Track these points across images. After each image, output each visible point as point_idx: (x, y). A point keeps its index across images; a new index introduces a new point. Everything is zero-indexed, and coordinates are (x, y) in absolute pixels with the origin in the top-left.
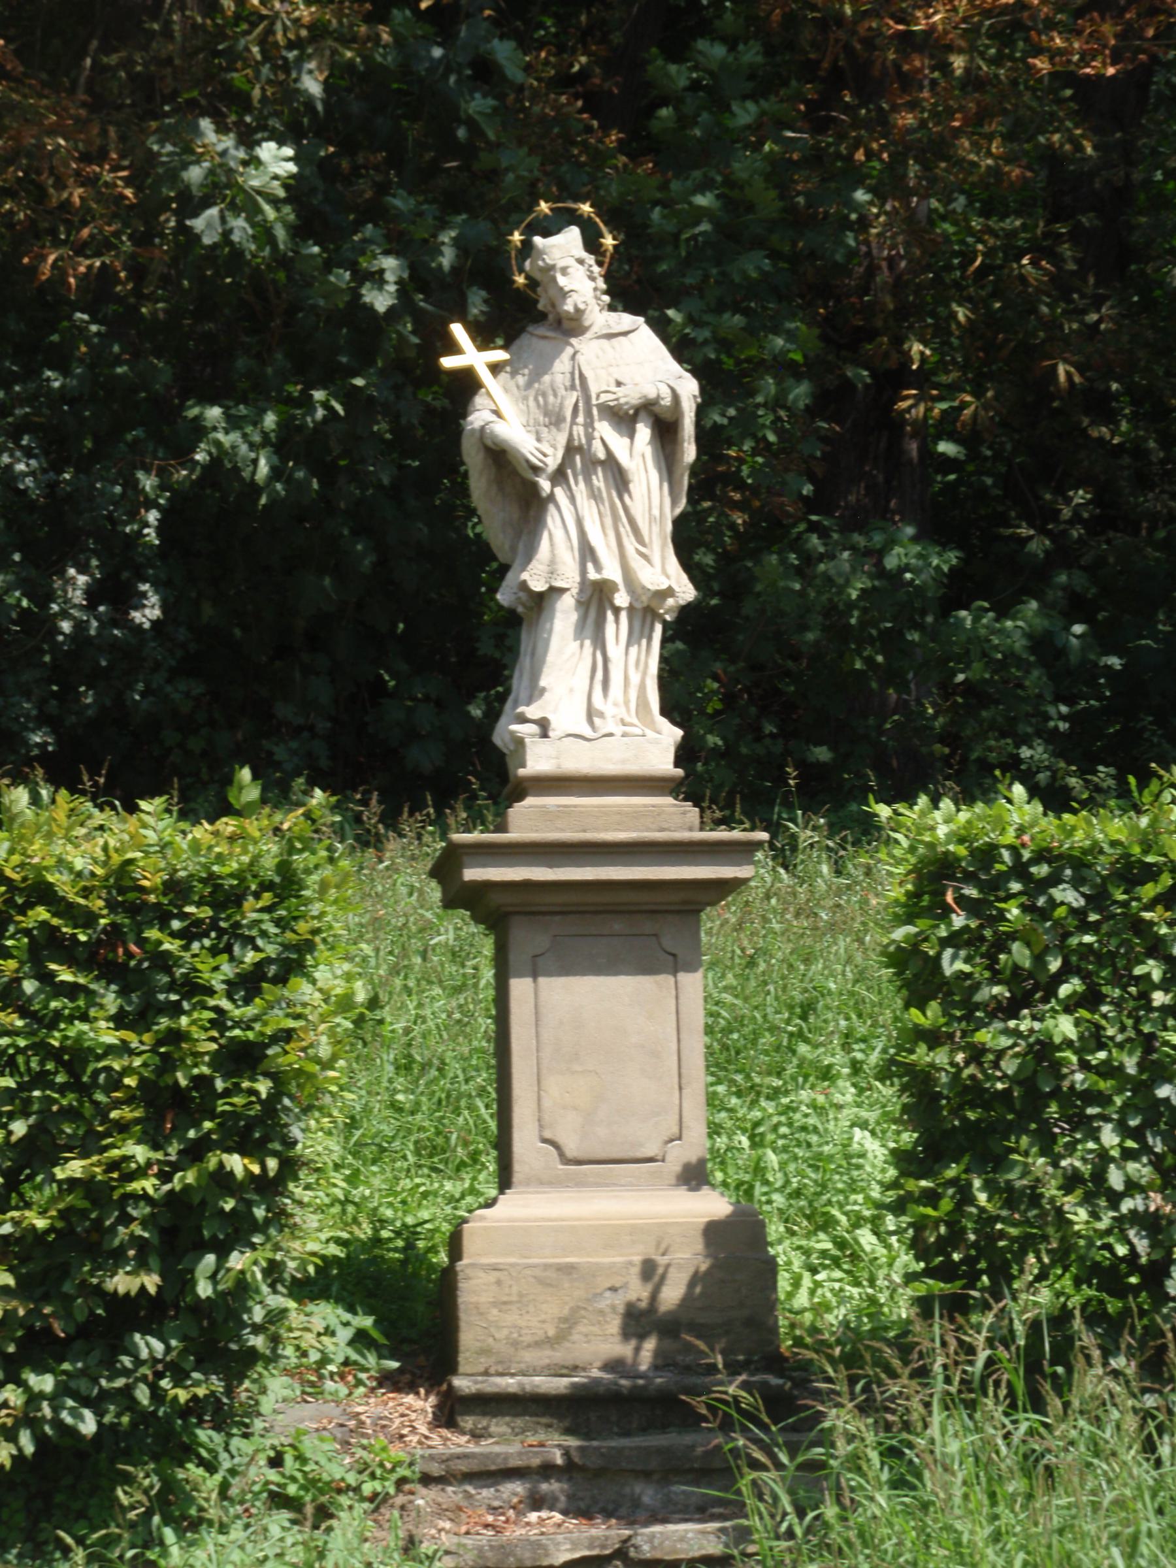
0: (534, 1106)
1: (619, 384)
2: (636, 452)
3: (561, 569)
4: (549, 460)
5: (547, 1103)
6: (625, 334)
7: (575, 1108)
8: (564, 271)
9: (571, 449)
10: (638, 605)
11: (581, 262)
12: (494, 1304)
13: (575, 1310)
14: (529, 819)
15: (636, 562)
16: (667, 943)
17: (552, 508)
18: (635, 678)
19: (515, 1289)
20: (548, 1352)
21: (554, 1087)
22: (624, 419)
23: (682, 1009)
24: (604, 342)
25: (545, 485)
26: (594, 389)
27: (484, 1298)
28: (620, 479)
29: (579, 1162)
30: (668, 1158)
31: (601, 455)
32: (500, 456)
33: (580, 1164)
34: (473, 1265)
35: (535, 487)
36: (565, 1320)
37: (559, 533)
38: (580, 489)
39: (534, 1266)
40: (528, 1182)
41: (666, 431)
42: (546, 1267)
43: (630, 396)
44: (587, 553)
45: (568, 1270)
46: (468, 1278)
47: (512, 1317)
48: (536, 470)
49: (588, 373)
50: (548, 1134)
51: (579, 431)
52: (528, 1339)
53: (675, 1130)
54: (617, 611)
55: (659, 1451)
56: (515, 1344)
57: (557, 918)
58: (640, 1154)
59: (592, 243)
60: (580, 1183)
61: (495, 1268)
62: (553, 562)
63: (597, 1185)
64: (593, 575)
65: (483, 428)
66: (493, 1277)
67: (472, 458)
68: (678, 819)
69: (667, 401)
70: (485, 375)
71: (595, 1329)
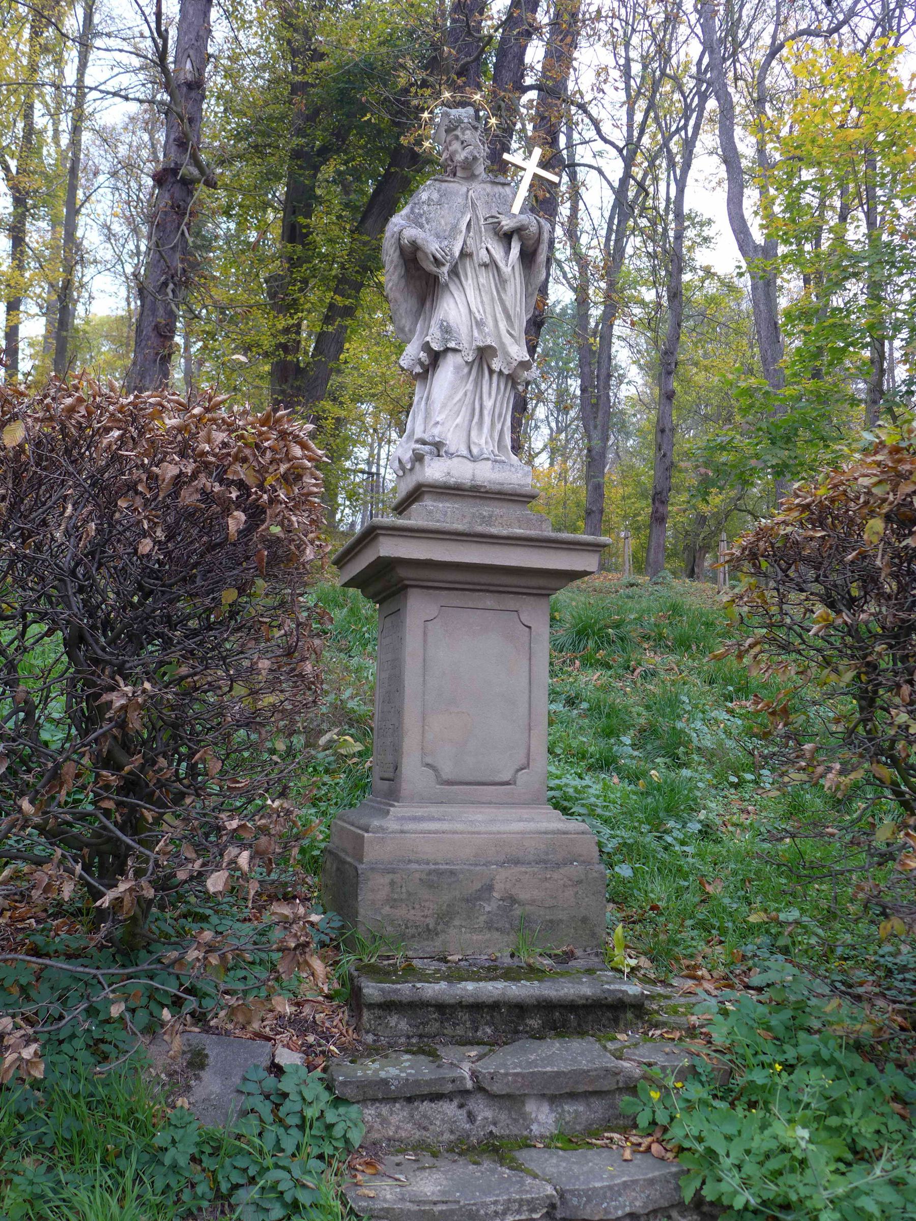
10: (506, 372)
16: (525, 618)
18: (499, 427)
28: (501, 281)
35: (436, 278)
48: (438, 263)
50: (429, 760)
53: (524, 761)
54: (491, 372)
58: (497, 779)
67: (390, 255)
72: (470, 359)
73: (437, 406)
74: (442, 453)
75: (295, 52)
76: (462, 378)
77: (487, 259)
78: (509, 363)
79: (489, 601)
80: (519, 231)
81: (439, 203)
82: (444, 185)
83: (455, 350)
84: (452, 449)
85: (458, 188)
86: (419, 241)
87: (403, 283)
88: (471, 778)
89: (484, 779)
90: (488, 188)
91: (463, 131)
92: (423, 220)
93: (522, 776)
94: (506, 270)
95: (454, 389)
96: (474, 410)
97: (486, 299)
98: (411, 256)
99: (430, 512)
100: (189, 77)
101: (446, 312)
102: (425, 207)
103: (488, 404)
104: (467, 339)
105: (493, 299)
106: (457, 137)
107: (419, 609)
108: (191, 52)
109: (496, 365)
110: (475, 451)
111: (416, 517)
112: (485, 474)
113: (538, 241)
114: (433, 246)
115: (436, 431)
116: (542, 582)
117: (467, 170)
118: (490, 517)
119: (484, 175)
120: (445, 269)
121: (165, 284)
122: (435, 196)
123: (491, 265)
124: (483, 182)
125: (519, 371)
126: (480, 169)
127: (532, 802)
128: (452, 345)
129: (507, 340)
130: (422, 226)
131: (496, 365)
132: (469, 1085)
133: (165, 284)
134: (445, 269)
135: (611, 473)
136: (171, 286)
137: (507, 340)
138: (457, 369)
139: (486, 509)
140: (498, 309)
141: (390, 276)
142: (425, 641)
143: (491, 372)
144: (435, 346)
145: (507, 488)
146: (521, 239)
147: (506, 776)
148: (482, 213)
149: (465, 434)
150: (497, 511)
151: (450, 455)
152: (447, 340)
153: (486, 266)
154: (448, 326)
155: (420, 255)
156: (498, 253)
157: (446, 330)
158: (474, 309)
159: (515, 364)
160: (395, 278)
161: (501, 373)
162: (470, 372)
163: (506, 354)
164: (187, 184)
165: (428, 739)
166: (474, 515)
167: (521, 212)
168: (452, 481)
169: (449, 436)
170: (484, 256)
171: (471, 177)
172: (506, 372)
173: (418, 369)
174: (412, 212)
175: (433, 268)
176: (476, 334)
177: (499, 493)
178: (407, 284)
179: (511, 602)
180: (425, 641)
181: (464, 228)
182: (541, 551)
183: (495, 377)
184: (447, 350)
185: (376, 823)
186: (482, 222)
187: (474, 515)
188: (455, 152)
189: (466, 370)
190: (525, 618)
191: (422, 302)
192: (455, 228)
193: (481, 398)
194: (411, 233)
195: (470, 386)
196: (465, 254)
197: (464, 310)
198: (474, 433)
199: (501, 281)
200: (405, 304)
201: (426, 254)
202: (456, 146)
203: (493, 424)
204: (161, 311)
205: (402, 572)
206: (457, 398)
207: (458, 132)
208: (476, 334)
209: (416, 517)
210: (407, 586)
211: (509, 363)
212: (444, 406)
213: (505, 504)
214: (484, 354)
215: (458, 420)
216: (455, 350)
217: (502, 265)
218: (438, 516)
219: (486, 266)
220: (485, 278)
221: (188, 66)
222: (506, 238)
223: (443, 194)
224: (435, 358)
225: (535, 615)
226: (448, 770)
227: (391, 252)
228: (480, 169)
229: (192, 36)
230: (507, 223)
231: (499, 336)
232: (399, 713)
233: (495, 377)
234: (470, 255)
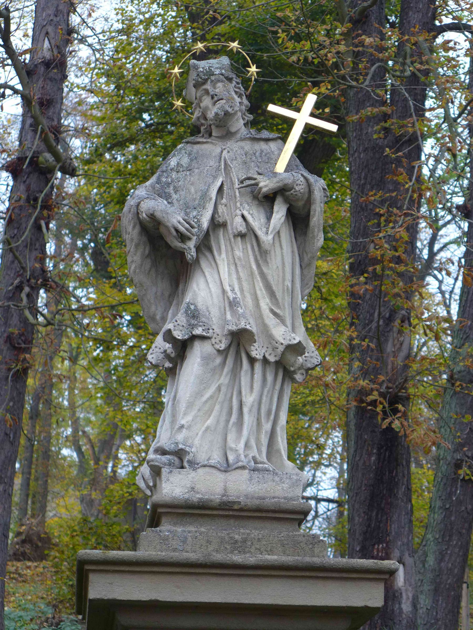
10: (272, 359)
18: (267, 427)
28: (262, 253)
35: (181, 254)
48: (183, 238)
54: (252, 361)
72: (222, 346)
73: (182, 406)
74: (186, 464)
75: (193, 18)
76: (214, 370)
77: (242, 228)
80: (282, 192)
81: (189, 169)
82: (196, 147)
83: (203, 338)
84: (202, 458)
85: (211, 149)
86: (158, 214)
87: (148, 264)
90: (247, 146)
91: (214, 84)
92: (171, 190)
94: (267, 239)
95: (203, 383)
96: (231, 408)
98: (153, 232)
99: (166, 539)
100: (48, 55)
101: (195, 294)
102: (174, 175)
103: (249, 399)
104: (218, 322)
105: (252, 274)
106: (207, 92)
108: (50, 29)
109: (257, 351)
110: (231, 458)
111: (151, 546)
112: (241, 487)
113: (309, 202)
114: (175, 218)
115: (180, 437)
117: (221, 128)
118: (244, 541)
119: (244, 131)
120: (191, 244)
121: (20, 288)
122: (185, 161)
123: (248, 234)
124: (242, 140)
125: (290, 358)
126: (238, 125)
128: (198, 331)
129: (271, 320)
130: (167, 197)
133: (20, 288)
134: (191, 244)
136: (27, 289)
137: (271, 320)
138: (206, 359)
139: (240, 532)
140: (259, 285)
143: (252, 361)
144: (179, 335)
145: (268, 503)
146: (286, 200)
148: (237, 174)
149: (219, 439)
150: (255, 533)
151: (193, 464)
152: (193, 327)
153: (242, 236)
154: (196, 309)
155: (162, 230)
156: (256, 219)
157: (194, 315)
158: (227, 288)
161: (265, 361)
162: (224, 362)
163: (270, 337)
164: (45, 173)
166: (222, 541)
167: (286, 171)
168: (196, 497)
169: (197, 442)
170: (238, 224)
171: (228, 135)
172: (272, 359)
173: (168, 365)
174: (159, 181)
175: (177, 244)
176: (229, 317)
177: (258, 510)
178: (155, 264)
181: (213, 193)
182: (304, 583)
183: (258, 367)
184: (194, 338)
186: (237, 186)
187: (222, 541)
188: (207, 108)
189: (218, 360)
192: (205, 196)
193: (240, 393)
194: (148, 206)
195: (224, 379)
196: (217, 225)
197: (215, 289)
198: (231, 437)
199: (262, 253)
200: (155, 288)
201: (167, 227)
202: (207, 102)
204: (15, 320)
206: (207, 395)
207: (208, 86)
208: (229, 317)
209: (151, 546)
212: (190, 405)
213: (268, 524)
214: (239, 340)
215: (209, 422)
216: (203, 338)
217: (260, 233)
218: (175, 543)
219: (242, 236)
220: (241, 250)
221: (46, 44)
222: (267, 200)
223: (193, 158)
224: (182, 348)
227: (130, 229)
228: (238, 125)
229: (51, 11)
230: (266, 184)
231: (260, 317)
233: (258, 367)
234: (224, 225)
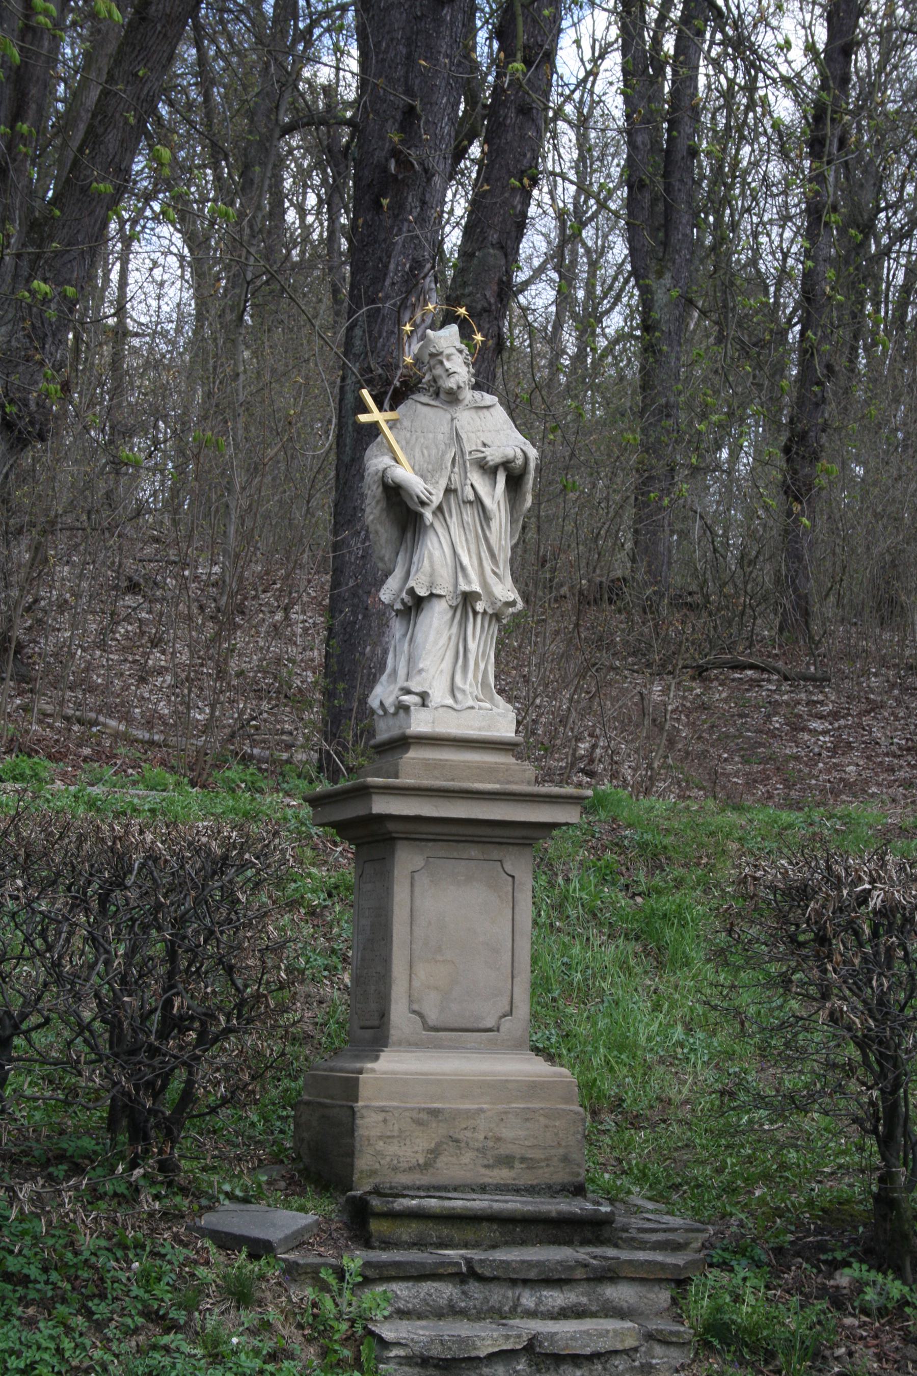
0: (407, 985)
1: (485, 445)
2: (494, 495)
3: (439, 581)
4: (434, 498)
5: (416, 984)
6: (488, 407)
7: (436, 988)
8: (449, 357)
9: (449, 491)
10: (490, 611)
11: (461, 352)
12: (381, 1138)
13: (438, 1145)
14: (414, 766)
15: (491, 579)
16: (508, 867)
17: (431, 534)
18: (482, 666)
19: (396, 1127)
20: (418, 1176)
21: (422, 972)
22: (489, 470)
23: (517, 917)
24: (473, 412)
25: (428, 515)
26: (467, 448)
27: (374, 1133)
28: (485, 515)
29: (437, 1029)
30: (502, 1029)
31: (471, 497)
32: (394, 494)
33: (440, 1033)
34: (367, 1107)
35: (420, 516)
36: (431, 1151)
37: (437, 553)
38: (454, 522)
39: (413, 1109)
40: (400, 1043)
41: (515, 481)
42: (421, 1110)
43: (494, 455)
44: (459, 567)
45: (435, 1113)
46: (362, 1117)
47: (393, 1149)
48: (423, 504)
49: (463, 436)
50: (416, 1007)
51: (456, 478)
52: (404, 1165)
53: (507, 1008)
54: (475, 613)
55: (538, 1264)
56: (395, 1169)
57: (430, 844)
58: (481, 1026)
59: (466, 334)
60: (438, 1046)
61: (383, 1110)
62: (432, 575)
63: (450, 1047)
64: (464, 587)
65: (385, 470)
66: (380, 1117)
67: (372, 492)
68: (520, 774)
69: (520, 462)
70: (385, 427)
71: (454, 1160)
77: (471, 497)
78: (493, 603)
79: (474, 852)
88: (456, 1025)
89: (469, 1026)
93: (506, 1024)
97: (472, 538)
103: (472, 645)
105: (477, 536)
107: (407, 861)
116: (524, 833)
127: (515, 1046)
131: (479, 607)
132: (464, 1269)
135: (521, 1182)
140: (484, 547)
141: (373, 511)
142: (412, 892)
144: (422, 592)
147: (490, 1023)
153: (470, 503)
156: (483, 489)
159: (499, 604)
160: (377, 512)
165: (415, 984)
172: (490, 611)
179: (496, 853)
180: (412, 892)
181: (449, 464)
184: (432, 595)
185: (369, 1065)
189: (450, 614)
190: (508, 867)
191: (403, 531)
203: (476, 664)
205: (391, 826)
210: (395, 839)
211: (493, 603)
216: (440, 596)
217: (487, 501)
225: (520, 866)
226: (433, 1017)
232: (387, 961)
